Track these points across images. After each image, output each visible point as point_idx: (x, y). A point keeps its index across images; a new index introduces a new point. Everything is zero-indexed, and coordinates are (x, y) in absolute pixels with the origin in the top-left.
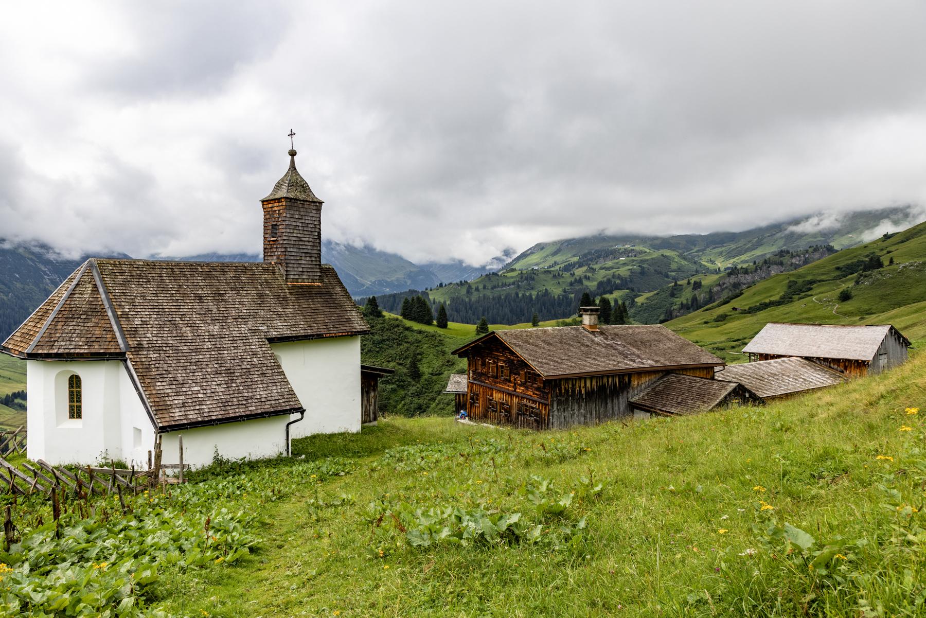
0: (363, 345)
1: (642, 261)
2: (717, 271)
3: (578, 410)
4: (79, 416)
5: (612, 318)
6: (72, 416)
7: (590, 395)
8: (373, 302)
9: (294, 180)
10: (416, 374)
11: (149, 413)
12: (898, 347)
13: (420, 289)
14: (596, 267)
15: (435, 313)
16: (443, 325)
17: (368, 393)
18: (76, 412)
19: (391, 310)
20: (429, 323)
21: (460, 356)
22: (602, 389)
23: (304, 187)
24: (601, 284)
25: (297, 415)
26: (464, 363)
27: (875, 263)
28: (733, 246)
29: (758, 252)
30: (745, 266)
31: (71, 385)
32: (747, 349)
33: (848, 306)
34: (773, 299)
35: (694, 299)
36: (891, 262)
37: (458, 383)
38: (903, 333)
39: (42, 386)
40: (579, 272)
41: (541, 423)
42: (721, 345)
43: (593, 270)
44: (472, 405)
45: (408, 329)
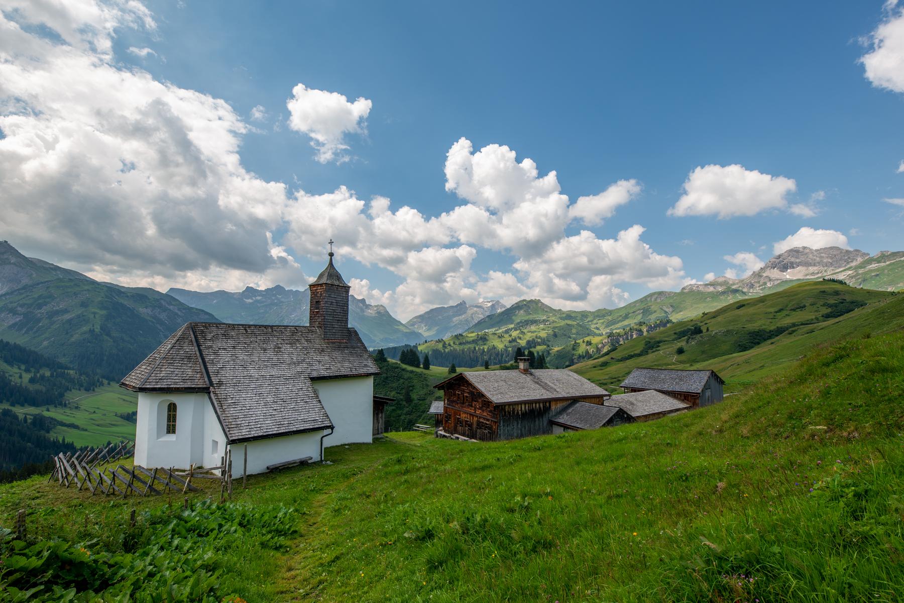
0: (375, 380)
1: (555, 328)
2: (601, 335)
3: (516, 427)
4: (174, 432)
5: (536, 364)
6: (168, 432)
7: (525, 416)
8: (381, 352)
9: (332, 272)
10: (409, 400)
11: (224, 430)
12: (717, 385)
13: (412, 344)
14: (525, 331)
15: (422, 360)
16: (427, 367)
17: (378, 414)
18: (171, 429)
19: (393, 358)
20: (418, 366)
21: (439, 389)
22: (532, 411)
23: (339, 277)
24: (528, 342)
25: (329, 431)
26: (441, 393)
27: (697, 331)
28: (610, 318)
29: (626, 323)
30: (618, 331)
31: (169, 410)
32: (623, 384)
33: (683, 357)
34: (636, 352)
35: (587, 352)
36: (708, 330)
37: (437, 407)
38: (719, 375)
39: (148, 412)
40: (515, 334)
41: (492, 436)
42: (605, 382)
43: (523, 333)
44: (446, 421)
45: (403, 370)
